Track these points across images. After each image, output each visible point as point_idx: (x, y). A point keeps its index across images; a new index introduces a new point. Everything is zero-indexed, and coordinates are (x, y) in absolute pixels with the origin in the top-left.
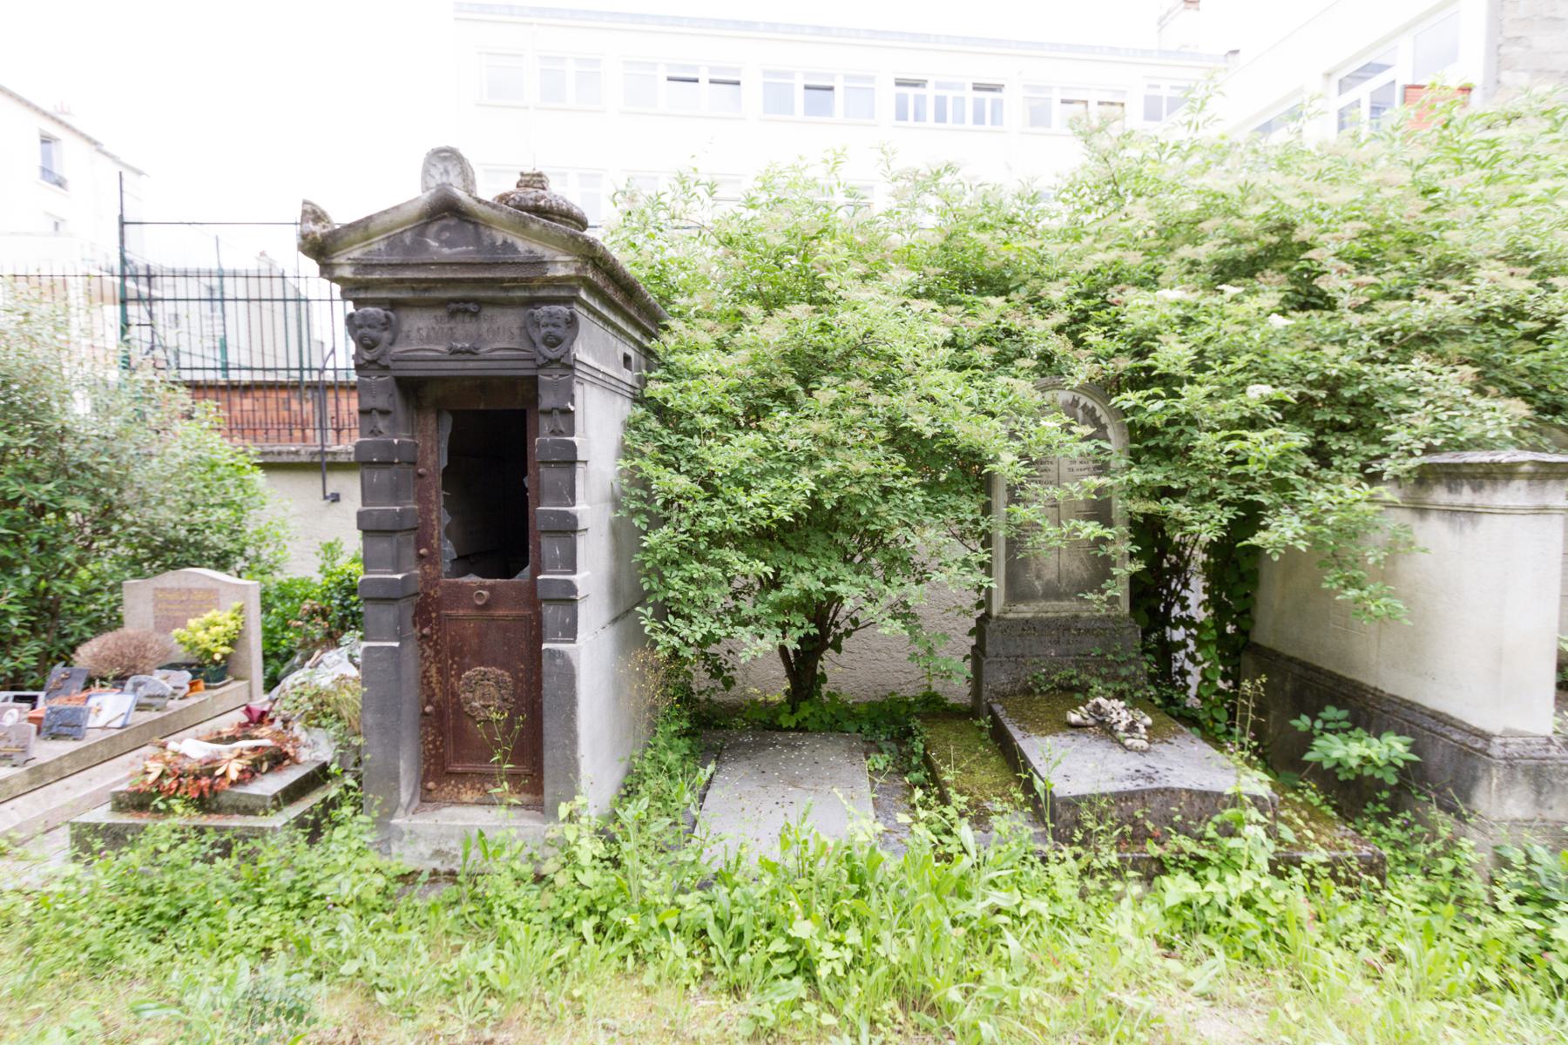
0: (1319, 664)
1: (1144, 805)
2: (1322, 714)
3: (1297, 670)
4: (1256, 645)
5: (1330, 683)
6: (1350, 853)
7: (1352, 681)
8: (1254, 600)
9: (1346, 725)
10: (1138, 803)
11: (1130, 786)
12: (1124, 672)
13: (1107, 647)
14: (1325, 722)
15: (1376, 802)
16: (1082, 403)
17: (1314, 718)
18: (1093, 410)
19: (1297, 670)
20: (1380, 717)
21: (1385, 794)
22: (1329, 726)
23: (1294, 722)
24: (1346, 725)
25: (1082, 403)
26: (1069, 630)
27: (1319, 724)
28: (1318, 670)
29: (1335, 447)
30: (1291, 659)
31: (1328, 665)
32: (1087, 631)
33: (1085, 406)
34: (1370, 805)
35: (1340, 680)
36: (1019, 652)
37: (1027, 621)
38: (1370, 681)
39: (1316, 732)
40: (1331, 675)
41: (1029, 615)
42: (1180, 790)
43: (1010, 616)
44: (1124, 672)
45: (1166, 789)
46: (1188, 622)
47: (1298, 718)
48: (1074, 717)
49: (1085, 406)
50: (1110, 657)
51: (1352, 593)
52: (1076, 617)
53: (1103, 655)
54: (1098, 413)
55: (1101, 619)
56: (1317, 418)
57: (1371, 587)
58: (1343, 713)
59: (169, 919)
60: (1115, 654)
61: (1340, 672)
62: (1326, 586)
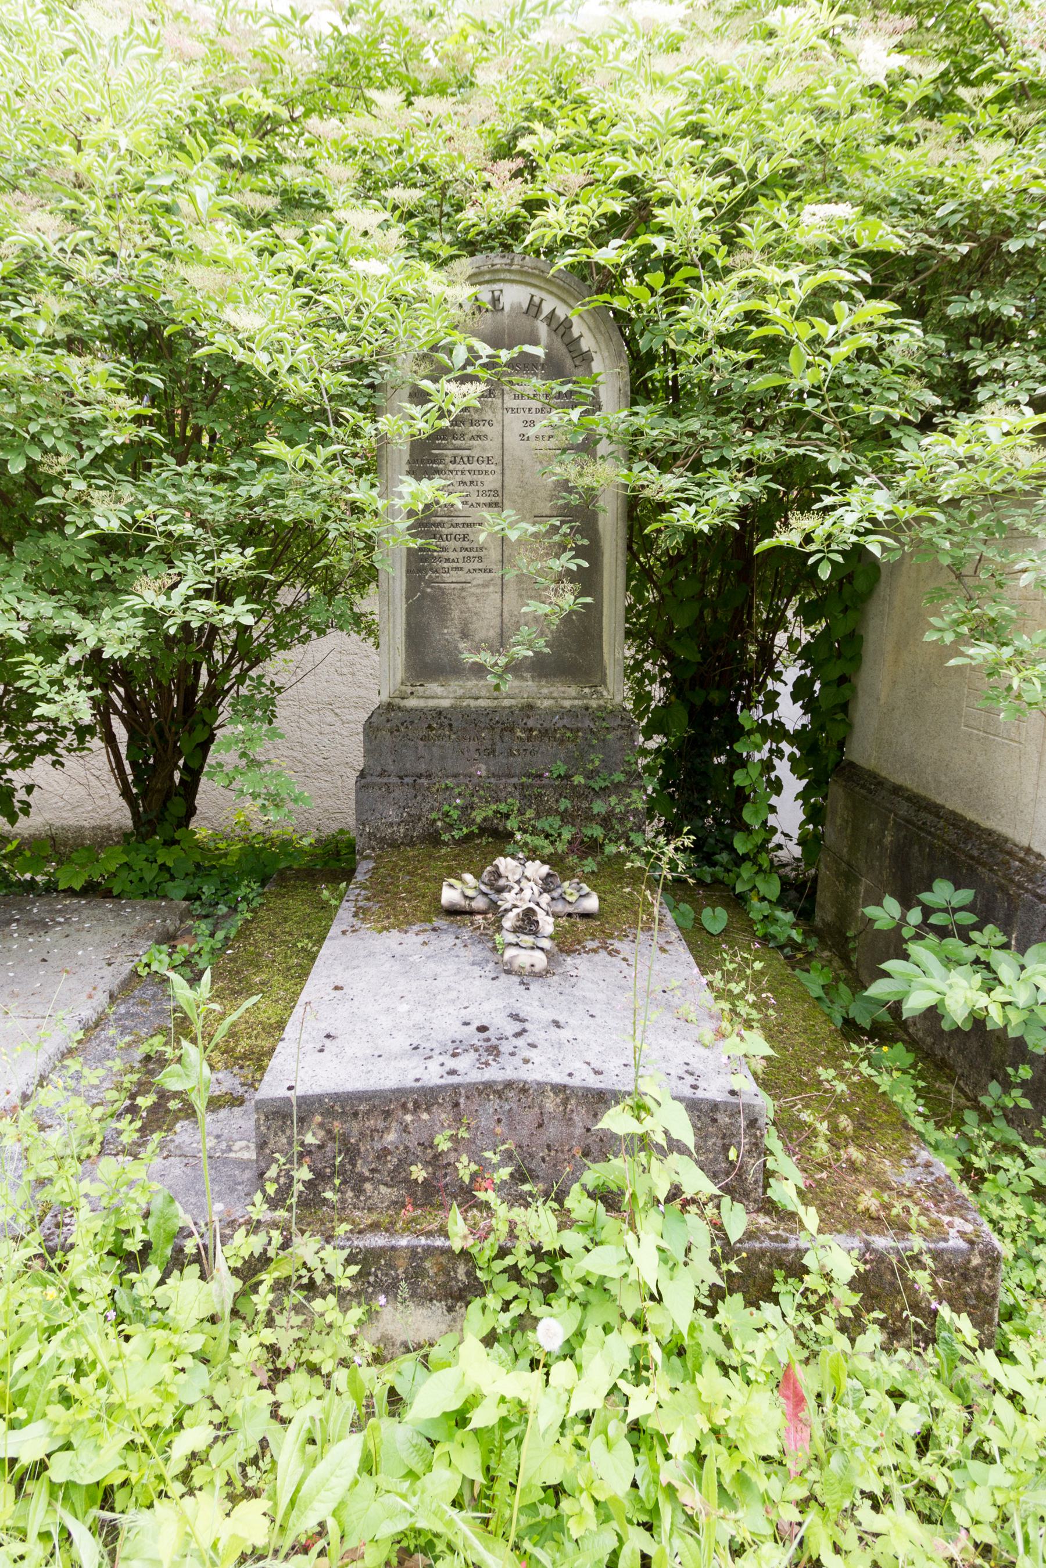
0: (939, 801)
1: (458, 1120)
2: (925, 897)
3: (904, 809)
4: (852, 765)
5: (951, 835)
6: (917, 1243)
7: (990, 832)
8: (854, 690)
9: (967, 918)
10: (444, 1116)
11: (433, 1075)
12: (599, 807)
13: (576, 761)
14: (928, 911)
15: (1007, 1086)
16: (546, 309)
17: (907, 904)
18: (567, 324)
19: (904, 809)
20: (1031, 908)
21: (1025, 1072)
22: (935, 920)
23: (871, 911)
24: (967, 918)
25: (546, 309)
26: (512, 730)
27: (915, 916)
28: (935, 809)
29: (981, 372)
30: (897, 790)
31: (954, 803)
32: (545, 733)
33: (552, 314)
34: (994, 1088)
35: (970, 830)
36: (422, 768)
37: (439, 713)
38: (1020, 836)
39: (907, 932)
40: (955, 820)
41: (445, 703)
42: (541, 1087)
43: (412, 703)
44: (599, 807)
45: (509, 1085)
46: (776, 731)
47: (879, 903)
48: (450, 895)
49: (552, 314)
50: (578, 779)
51: (982, 652)
52: (529, 708)
53: (567, 777)
54: (576, 332)
55: (571, 713)
56: (954, 311)
57: (1022, 641)
58: (966, 896)
59: (237, 938)
60: (590, 775)
61: (971, 816)
62: (931, 637)
